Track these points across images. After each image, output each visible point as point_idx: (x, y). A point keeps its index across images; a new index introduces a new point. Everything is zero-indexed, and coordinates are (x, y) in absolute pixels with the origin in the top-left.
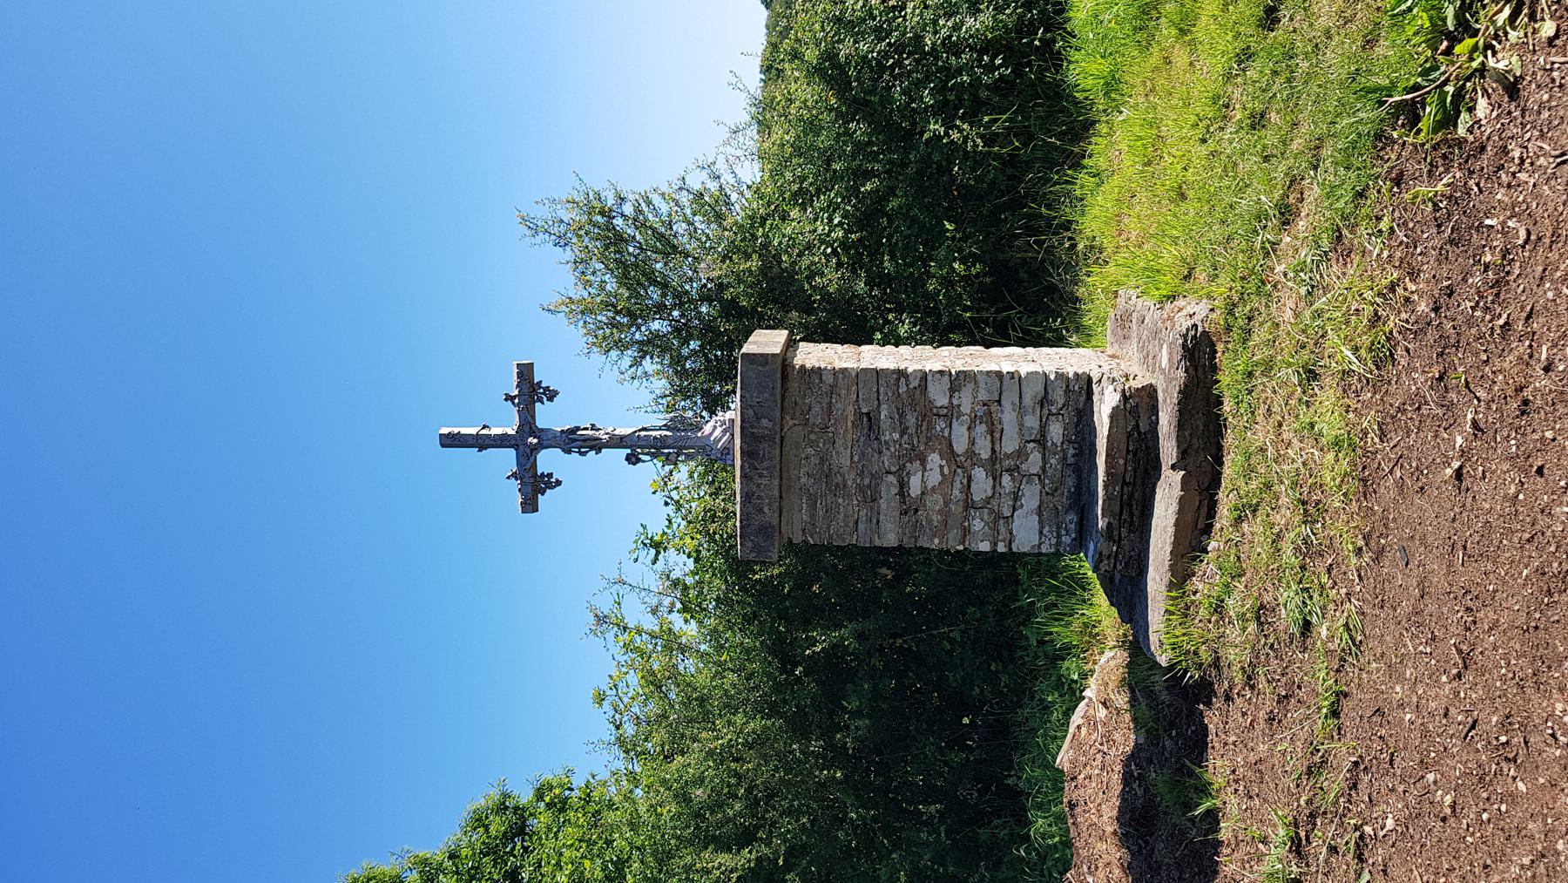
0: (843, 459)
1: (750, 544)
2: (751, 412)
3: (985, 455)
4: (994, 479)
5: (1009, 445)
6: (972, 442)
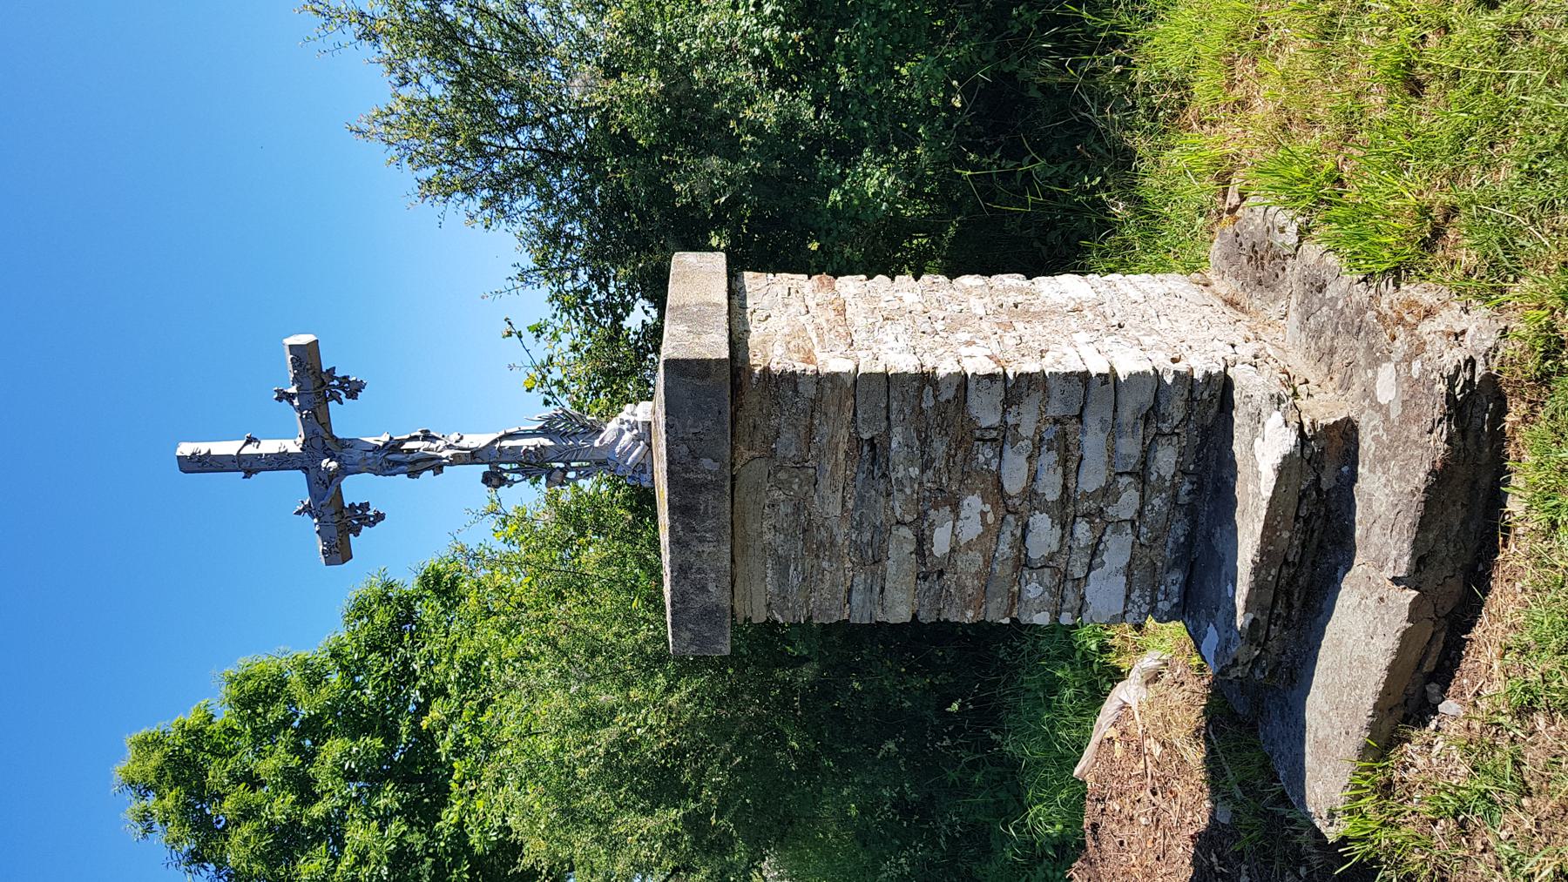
0: (830, 506)
1: (687, 635)
2: (684, 449)
3: (1052, 495)
4: (1063, 528)
5: (1091, 479)
6: (1033, 477)
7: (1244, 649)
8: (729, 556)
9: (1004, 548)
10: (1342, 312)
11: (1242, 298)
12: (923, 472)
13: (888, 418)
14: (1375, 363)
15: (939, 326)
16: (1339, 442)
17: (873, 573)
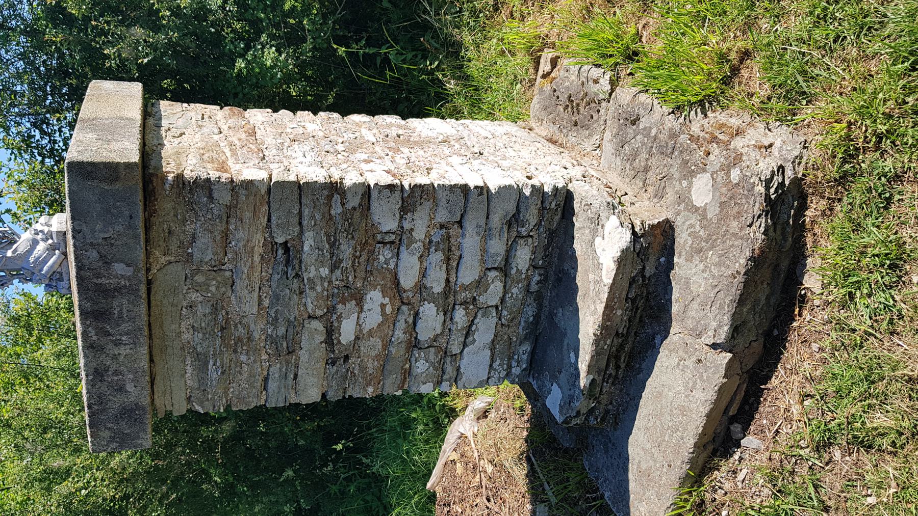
0: (246, 304)
2: (94, 255)
3: (438, 288)
4: (445, 314)
5: (468, 275)
6: (424, 274)
7: (585, 403)
8: (147, 357)
9: (399, 334)
10: (655, 138)
11: (561, 139)
12: (332, 271)
13: (300, 224)
14: (690, 174)
15: (340, 148)
16: (660, 238)
17: (288, 362)
